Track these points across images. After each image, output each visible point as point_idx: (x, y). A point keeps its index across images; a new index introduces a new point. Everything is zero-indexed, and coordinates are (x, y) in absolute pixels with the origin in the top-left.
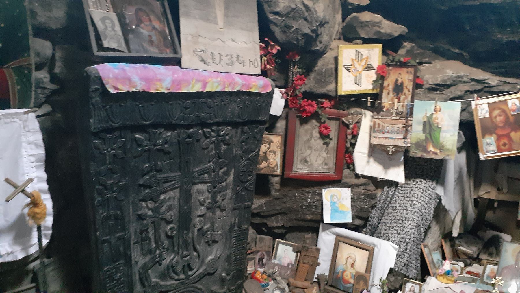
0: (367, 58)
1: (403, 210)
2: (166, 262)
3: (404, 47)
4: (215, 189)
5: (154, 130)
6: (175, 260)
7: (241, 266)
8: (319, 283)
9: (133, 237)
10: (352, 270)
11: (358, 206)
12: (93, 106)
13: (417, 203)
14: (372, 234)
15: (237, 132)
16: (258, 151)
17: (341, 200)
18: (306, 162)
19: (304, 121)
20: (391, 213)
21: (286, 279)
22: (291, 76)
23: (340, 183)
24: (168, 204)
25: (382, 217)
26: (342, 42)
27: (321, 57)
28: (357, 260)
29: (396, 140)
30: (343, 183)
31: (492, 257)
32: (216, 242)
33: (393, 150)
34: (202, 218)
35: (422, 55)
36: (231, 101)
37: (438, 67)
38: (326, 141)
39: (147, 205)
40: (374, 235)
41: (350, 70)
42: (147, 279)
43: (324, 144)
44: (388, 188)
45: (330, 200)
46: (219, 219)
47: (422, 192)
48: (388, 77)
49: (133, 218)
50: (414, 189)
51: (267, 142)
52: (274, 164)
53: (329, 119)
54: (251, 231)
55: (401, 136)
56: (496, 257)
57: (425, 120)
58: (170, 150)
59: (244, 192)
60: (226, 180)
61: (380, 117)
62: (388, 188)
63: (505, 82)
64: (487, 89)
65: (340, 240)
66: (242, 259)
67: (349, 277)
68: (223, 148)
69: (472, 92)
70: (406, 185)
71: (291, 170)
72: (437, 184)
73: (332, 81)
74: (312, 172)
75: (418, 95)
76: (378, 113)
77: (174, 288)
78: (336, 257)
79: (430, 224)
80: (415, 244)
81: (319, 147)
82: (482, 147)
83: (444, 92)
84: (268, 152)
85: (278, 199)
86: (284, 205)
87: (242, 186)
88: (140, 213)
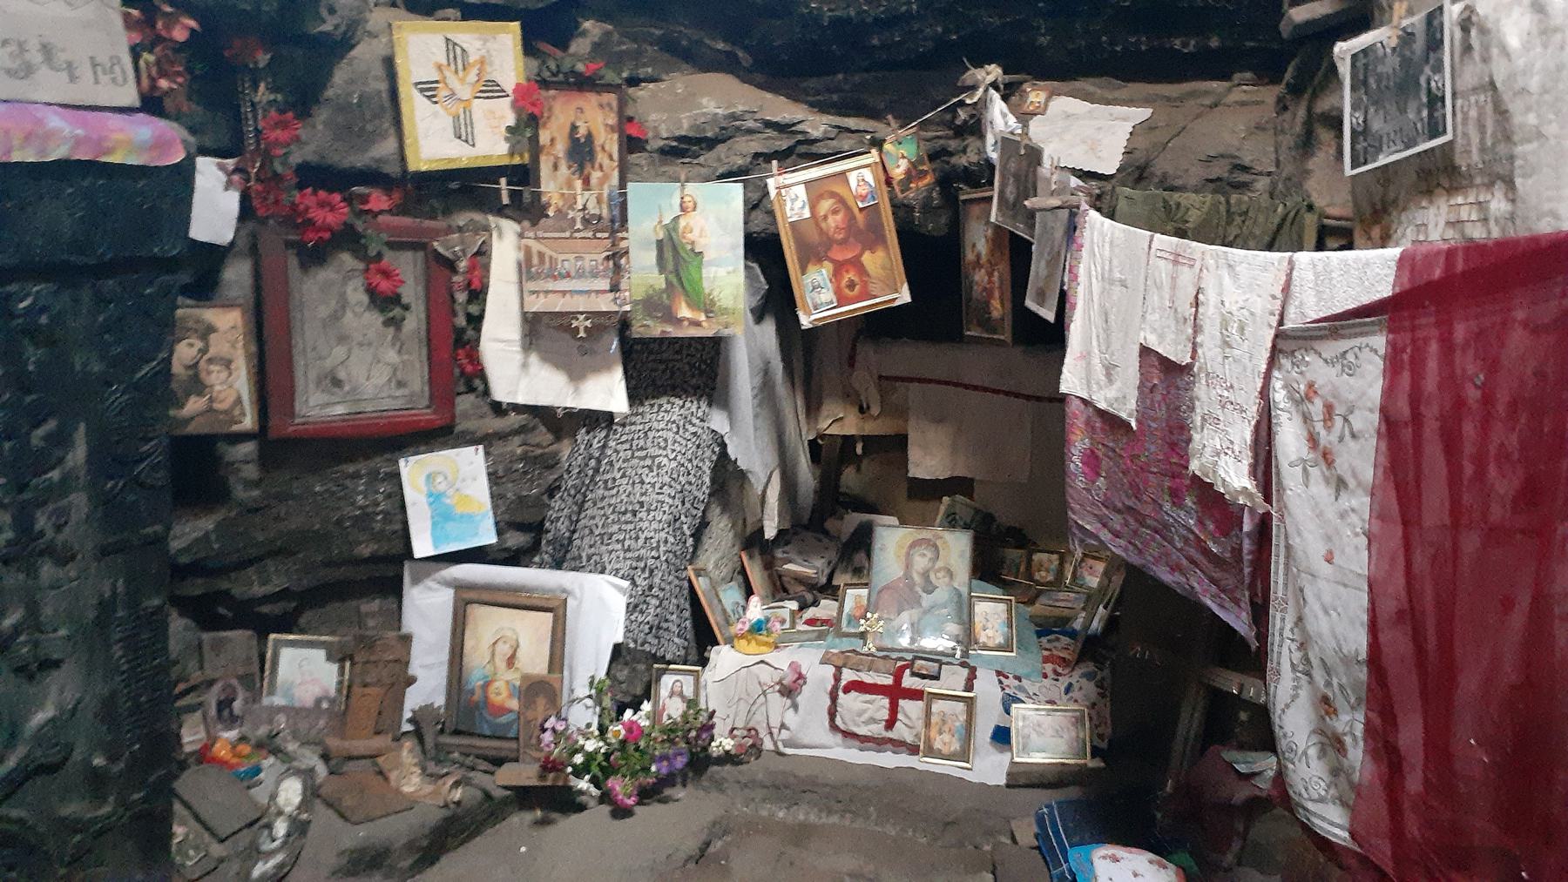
0: (482, 62)
1: (634, 483)
3: (584, 34)
4: (27, 496)
8: (418, 734)
11: (509, 495)
13: (665, 461)
14: (558, 565)
15: (76, 301)
16: (164, 359)
18: (337, 383)
19: (314, 257)
20: (603, 498)
21: (316, 744)
22: (250, 116)
25: (579, 513)
26: (402, 12)
27: (342, 57)
28: (521, 643)
31: (860, 578)
32: (57, 664)
35: (636, 56)
38: (391, 315)
41: (434, 96)
44: (588, 432)
45: (425, 489)
48: (549, 118)
50: (655, 425)
51: (196, 331)
52: (231, 399)
53: (393, 246)
54: (178, 625)
55: (604, 284)
57: (661, 236)
60: (61, 461)
61: (540, 234)
62: (588, 432)
64: (802, 149)
65: (467, 599)
67: (505, 694)
68: (33, 356)
69: (768, 158)
70: (634, 419)
71: (292, 414)
72: (710, 405)
73: (386, 131)
75: (638, 169)
76: (534, 224)
78: (462, 648)
79: (704, 512)
80: (672, 567)
81: (371, 334)
82: (803, 298)
83: (702, 159)
84: (202, 364)
85: (257, 510)
87: (121, 477)
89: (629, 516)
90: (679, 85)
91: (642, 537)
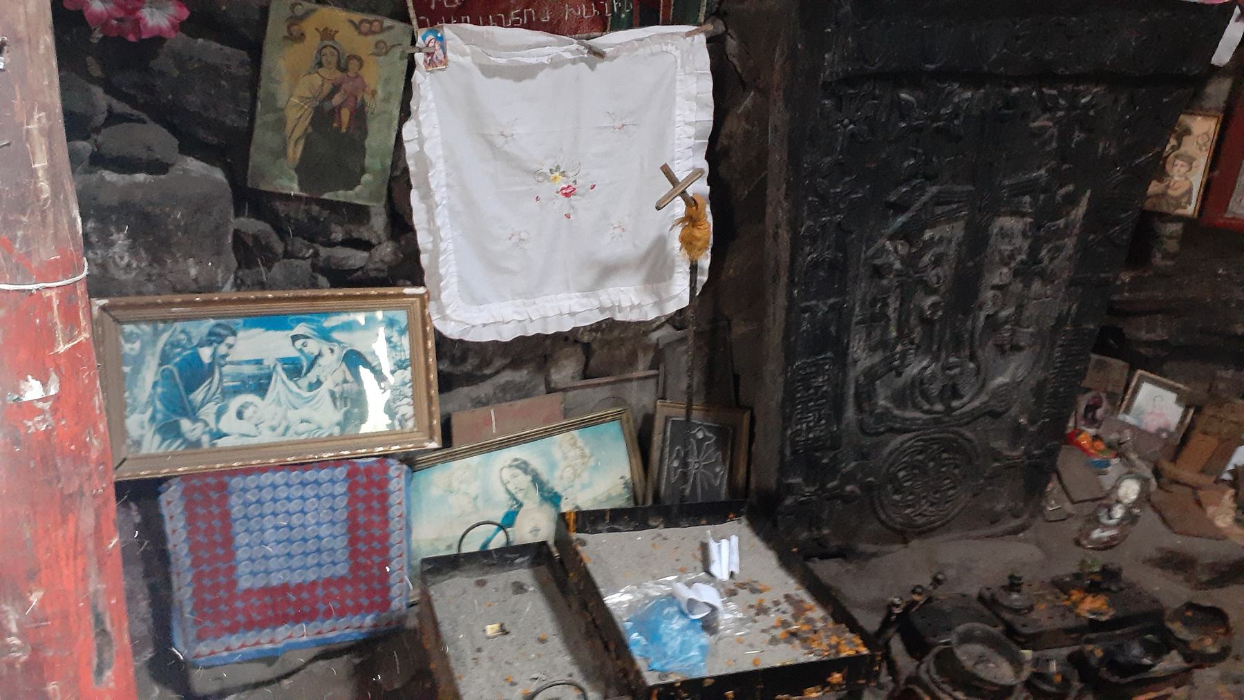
2: (913, 370)
6: (929, 371)
9: (858, 309)
15: (1116, 101)
24: (937, 250)
34: (998, 293)
60: (1068, 214)
68: (1078, 136)
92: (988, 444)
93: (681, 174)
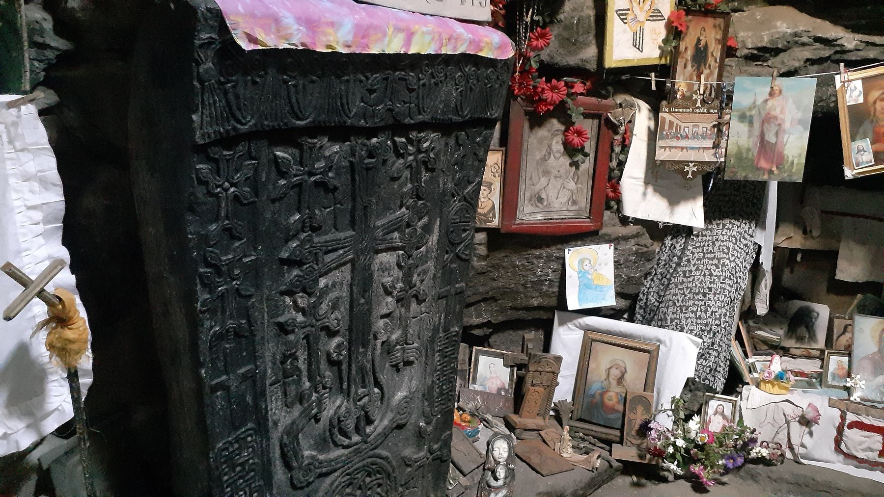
1: (704, 275)
2: (328, 413)
4: (411, 261)
5: (309, 140)
6: (343, 408)
7: (449, 404)
10: (618, 389)
12: (201, 82)
17: (597, 267)
18: (540, 200)
19: (537, 121)
20: (683, 282)
23: (598, 237)
24: (332, 295)
29: (702, 150)
30: (602, 234)
31: (802, 343)
33: (695, 169)
34: (386, 320)
36: (446, 78)
37: (758, 17)
39: (295, 302)
40: (652, 325)
41: (626, 19)
42: (296, 455)
43: (571, 165)
46: (414, 319)
47: (734, 242)
49: (269, 332)
52: (488, 208)
55: (709, 143)
56: (810, 343)
58: (336, 183)
59: (455, 263)
63: (868, 43)
66: (450, 391)
67: (615, 400)
68: (425, 176)
74: (551, 219)
77: (342, 464)
81: (562, 171)
82: (850, 157)
83: (770, 63)
86: (494, 284)
88: (281, 319)
89: (700, 296)
90: (758, 13)
91: (710, 311)
92: (400, 454)
93: (32, 271)
